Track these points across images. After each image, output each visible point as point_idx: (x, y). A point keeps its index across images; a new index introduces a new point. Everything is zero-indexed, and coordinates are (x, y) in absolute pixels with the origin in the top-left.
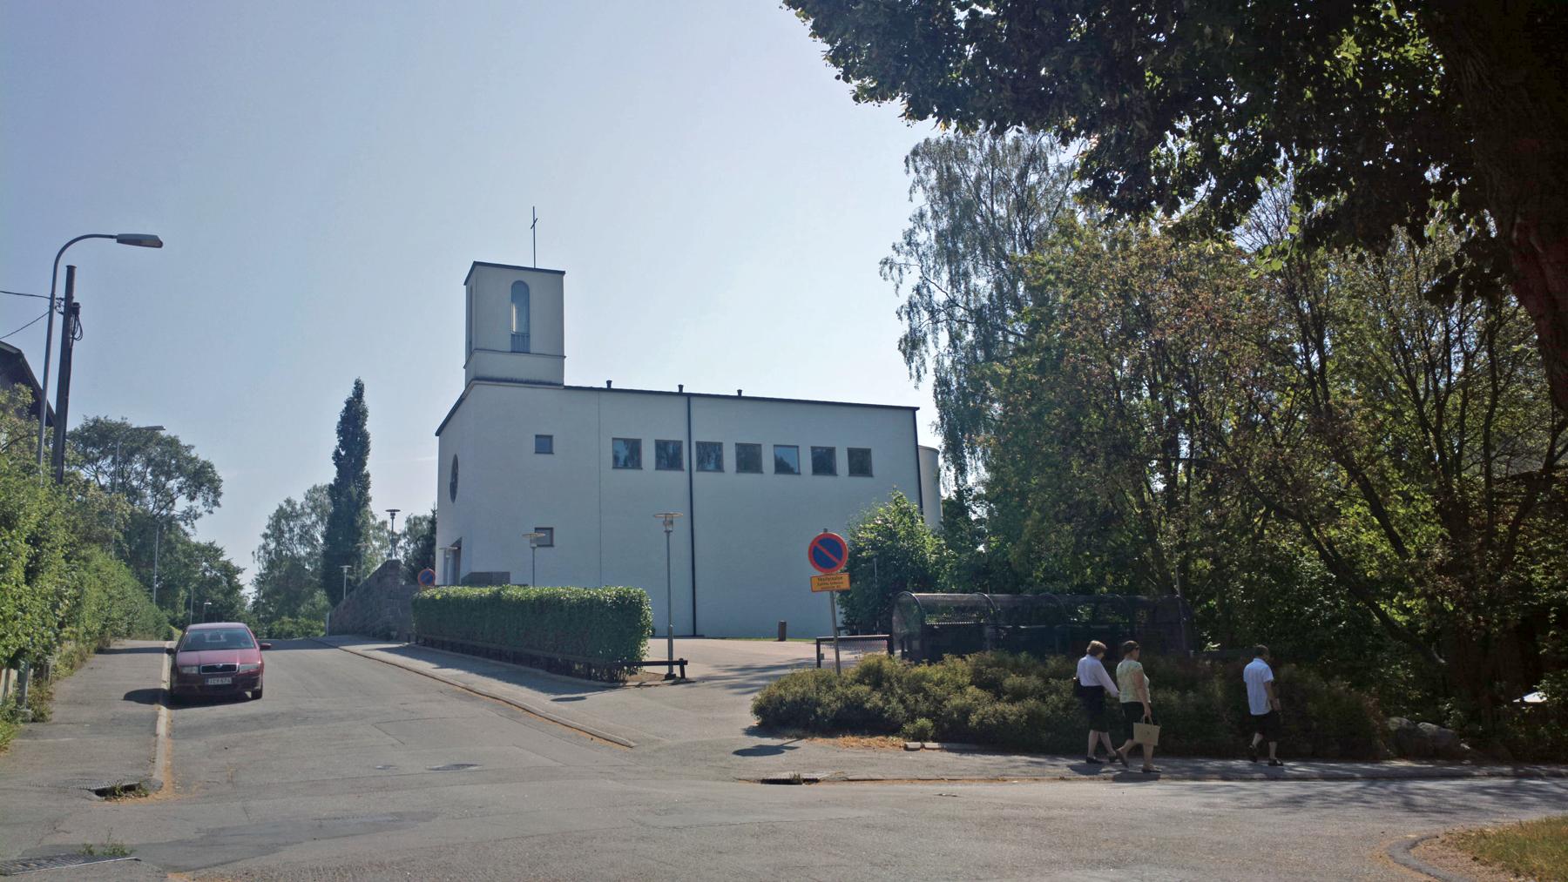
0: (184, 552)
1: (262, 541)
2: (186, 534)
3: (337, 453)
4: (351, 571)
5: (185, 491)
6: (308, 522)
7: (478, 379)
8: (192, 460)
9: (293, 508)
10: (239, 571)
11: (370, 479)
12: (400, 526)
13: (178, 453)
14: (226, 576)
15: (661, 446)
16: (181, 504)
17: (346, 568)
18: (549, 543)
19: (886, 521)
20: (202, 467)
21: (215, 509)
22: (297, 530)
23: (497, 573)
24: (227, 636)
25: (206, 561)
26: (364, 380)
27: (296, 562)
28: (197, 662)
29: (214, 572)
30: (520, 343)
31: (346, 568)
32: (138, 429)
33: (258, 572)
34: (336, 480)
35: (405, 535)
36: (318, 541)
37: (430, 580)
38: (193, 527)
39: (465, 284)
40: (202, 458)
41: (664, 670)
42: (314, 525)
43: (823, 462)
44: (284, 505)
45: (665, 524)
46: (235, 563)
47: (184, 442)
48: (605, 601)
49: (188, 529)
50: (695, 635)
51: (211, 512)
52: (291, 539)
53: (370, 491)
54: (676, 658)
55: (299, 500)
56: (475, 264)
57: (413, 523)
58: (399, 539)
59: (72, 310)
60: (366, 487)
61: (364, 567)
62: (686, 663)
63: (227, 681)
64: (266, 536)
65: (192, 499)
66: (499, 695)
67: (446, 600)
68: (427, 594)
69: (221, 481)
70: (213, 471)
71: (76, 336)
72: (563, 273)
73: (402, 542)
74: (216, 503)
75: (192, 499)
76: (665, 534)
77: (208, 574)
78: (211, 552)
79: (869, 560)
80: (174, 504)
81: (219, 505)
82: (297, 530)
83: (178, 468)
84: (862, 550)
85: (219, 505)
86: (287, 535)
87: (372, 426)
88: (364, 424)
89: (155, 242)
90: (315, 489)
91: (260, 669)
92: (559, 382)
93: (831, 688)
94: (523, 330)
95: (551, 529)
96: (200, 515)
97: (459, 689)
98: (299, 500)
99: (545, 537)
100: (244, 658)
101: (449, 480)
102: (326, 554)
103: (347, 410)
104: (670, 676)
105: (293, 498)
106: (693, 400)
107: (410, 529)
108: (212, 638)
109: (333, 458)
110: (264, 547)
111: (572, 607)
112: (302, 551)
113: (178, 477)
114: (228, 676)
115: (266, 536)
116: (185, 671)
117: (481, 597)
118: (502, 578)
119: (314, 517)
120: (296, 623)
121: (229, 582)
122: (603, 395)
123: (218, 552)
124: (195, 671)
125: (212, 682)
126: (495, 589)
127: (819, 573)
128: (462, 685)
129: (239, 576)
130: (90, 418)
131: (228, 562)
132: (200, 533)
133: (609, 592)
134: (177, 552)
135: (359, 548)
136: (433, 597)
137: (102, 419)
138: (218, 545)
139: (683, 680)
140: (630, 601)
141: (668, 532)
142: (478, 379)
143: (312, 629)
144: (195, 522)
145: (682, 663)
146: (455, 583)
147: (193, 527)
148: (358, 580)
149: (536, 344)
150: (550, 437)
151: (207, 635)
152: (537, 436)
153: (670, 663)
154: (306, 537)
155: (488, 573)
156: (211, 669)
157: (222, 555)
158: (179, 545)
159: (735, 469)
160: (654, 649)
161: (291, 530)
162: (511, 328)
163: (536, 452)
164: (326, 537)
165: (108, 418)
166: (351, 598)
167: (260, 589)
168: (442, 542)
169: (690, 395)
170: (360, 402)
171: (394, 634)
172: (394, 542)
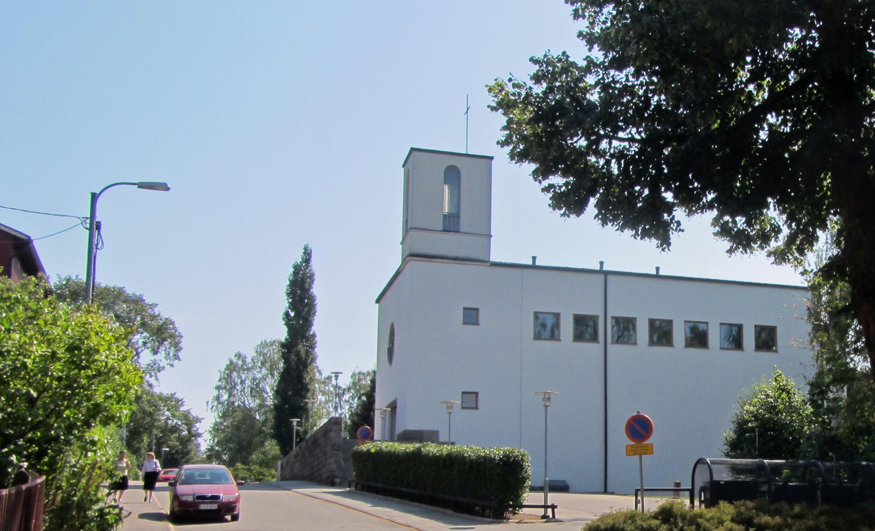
0: (149, 401)
1: (216, 393)
2: (151, 385)
3: (287, 314)
4: (299, 424)
5: (149, 345)
6: (259, 376)
7: (412, 255)
8: (154, 317)
9: (244, 361)
10: (198, 420)
11: (317, 339)
12: (345, 381)
13: (143, 310)
14: (187, 424)
15: (554, 336)
16: (146, 357)
17: (295, 421)
18: (474, 406)
19: (768, 396)
20: (164, 323)
21: (176, 362)
22: (248, 383)
23: (428, 431)
24: (211, 475)
25: (168, 410)
26: (311, 246)
27: (247, 413)
28: (192, 492)
29: (175, 421)
30: (451, 223)
31: (295, 421)
32: (107, 289)
33: (213, 421)
34: (286, 339)
35: (349, 389)
36: (267, 393)
37: (369, 436)
38: (157, 379)
39: (404, 166)
40: (165, 315)
41: (541, 511)
42: (264, 378)
43: (735, 340)
44: (235, 360)
45: (544, 399)
46: (194, 413)
47: (148, 300)
48: (494, 458)
49: (152, 380)
50: (606, 492)
51: (172, 365)
52: (243, 390)
53: (316, 350)
54: (549, 504)
55: (250, 354)
56: (413, 150)
57: (357, 377)
58: (343, 394)
59: (95, 227)
60: (313, 347)
61: (311, 420)
62: (556, 507)
63: (214, 507)
64: (218, 388)
65: (155, 352)
66: (412, 524)
67: (380, 454)
68: (365, 447)
69: (181, 337)
70: (174, 328)
71: (99, 247)
72: (491, 158)
73: (346, 397)
74: (176, 357)
75: (155, 352)
76: (544, 409)
77: (170, 422)
78: (172, 402)
79: (752, 430)
80: (139, 357)
81: (179, 359)
82: (248, 383)
83: (143, 325)
84: (747, 422)
85: (179, 359)
86: (239, 387)
87: (317, 289)
88: (310, 287)
89: (164, 187)
90: (264, 345)
91: (237, 500)
92: (486, 259)
93: (634, 521)
94: (454, 211)
95: (476, 393)
96: (163, 368)
97: (385, 521)
98: (250, 354)
99: (471, 399)
100: (227, 491)
101: (386, 346)
102: (277, 408)
103: (295, 274)
104: (545, 517)
105: (243, 352)
106: (610, 278)
107: (354, 384)
108: (200, 476)
109: (284, 319)
110: (218, 398)
111: (471, 461)
112: (253, 403)
113: (142, 333)
114: (215, 503)
115: (218, 388)
116: (184, 498)
117: (406, 452)
118: (432, 436)
119: (264, 371)
120: (249, 470)
121: (189, 431)
122: (526, 271)
123: (179, 402)
124: (190, 499)
125: (203, 507)
126: (418, 445)
127: (632, 443)
128: (388, 518)
129: (198, 425)
130: (63, 277)
131: (188, 412)
132: (162, 386)
133: (497, 451)
134: (143, 402)
135: (307, 403)
136: (368, 451)
137: (74, 278)
138: (179, 396)
139: (553, 519)
140: (514, 459)
141: (546, 407)
142: (412, 255)
143: (264, 475)
144: (158, 374)
145: (553, 507)
146: (392, 439)
147: (157, 379)
148: (306, 432)
149: (465, 224)
150: (477, 310)
151: (197, 473)
152: (465, 309)
153: (546, 507)
154: (257, 391)
155: (420, 431)
156: (202, 498)
157: (182, 405)
158: (145, 396)
159: (647, 344)
160: (529, 497)
161: (243, 382)
162: (442, 207)
163: (464, 323)
164: (279, 393)
165: (79, 277)
166: (300, 448)
167: (215, 436)
168: (381, 403)
169: (607, 273)
170: (307, 266)
171: (337, 480)
172: (339, 396)
